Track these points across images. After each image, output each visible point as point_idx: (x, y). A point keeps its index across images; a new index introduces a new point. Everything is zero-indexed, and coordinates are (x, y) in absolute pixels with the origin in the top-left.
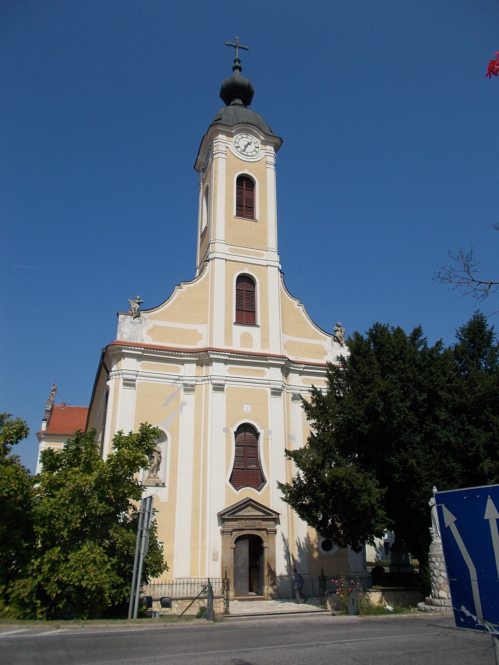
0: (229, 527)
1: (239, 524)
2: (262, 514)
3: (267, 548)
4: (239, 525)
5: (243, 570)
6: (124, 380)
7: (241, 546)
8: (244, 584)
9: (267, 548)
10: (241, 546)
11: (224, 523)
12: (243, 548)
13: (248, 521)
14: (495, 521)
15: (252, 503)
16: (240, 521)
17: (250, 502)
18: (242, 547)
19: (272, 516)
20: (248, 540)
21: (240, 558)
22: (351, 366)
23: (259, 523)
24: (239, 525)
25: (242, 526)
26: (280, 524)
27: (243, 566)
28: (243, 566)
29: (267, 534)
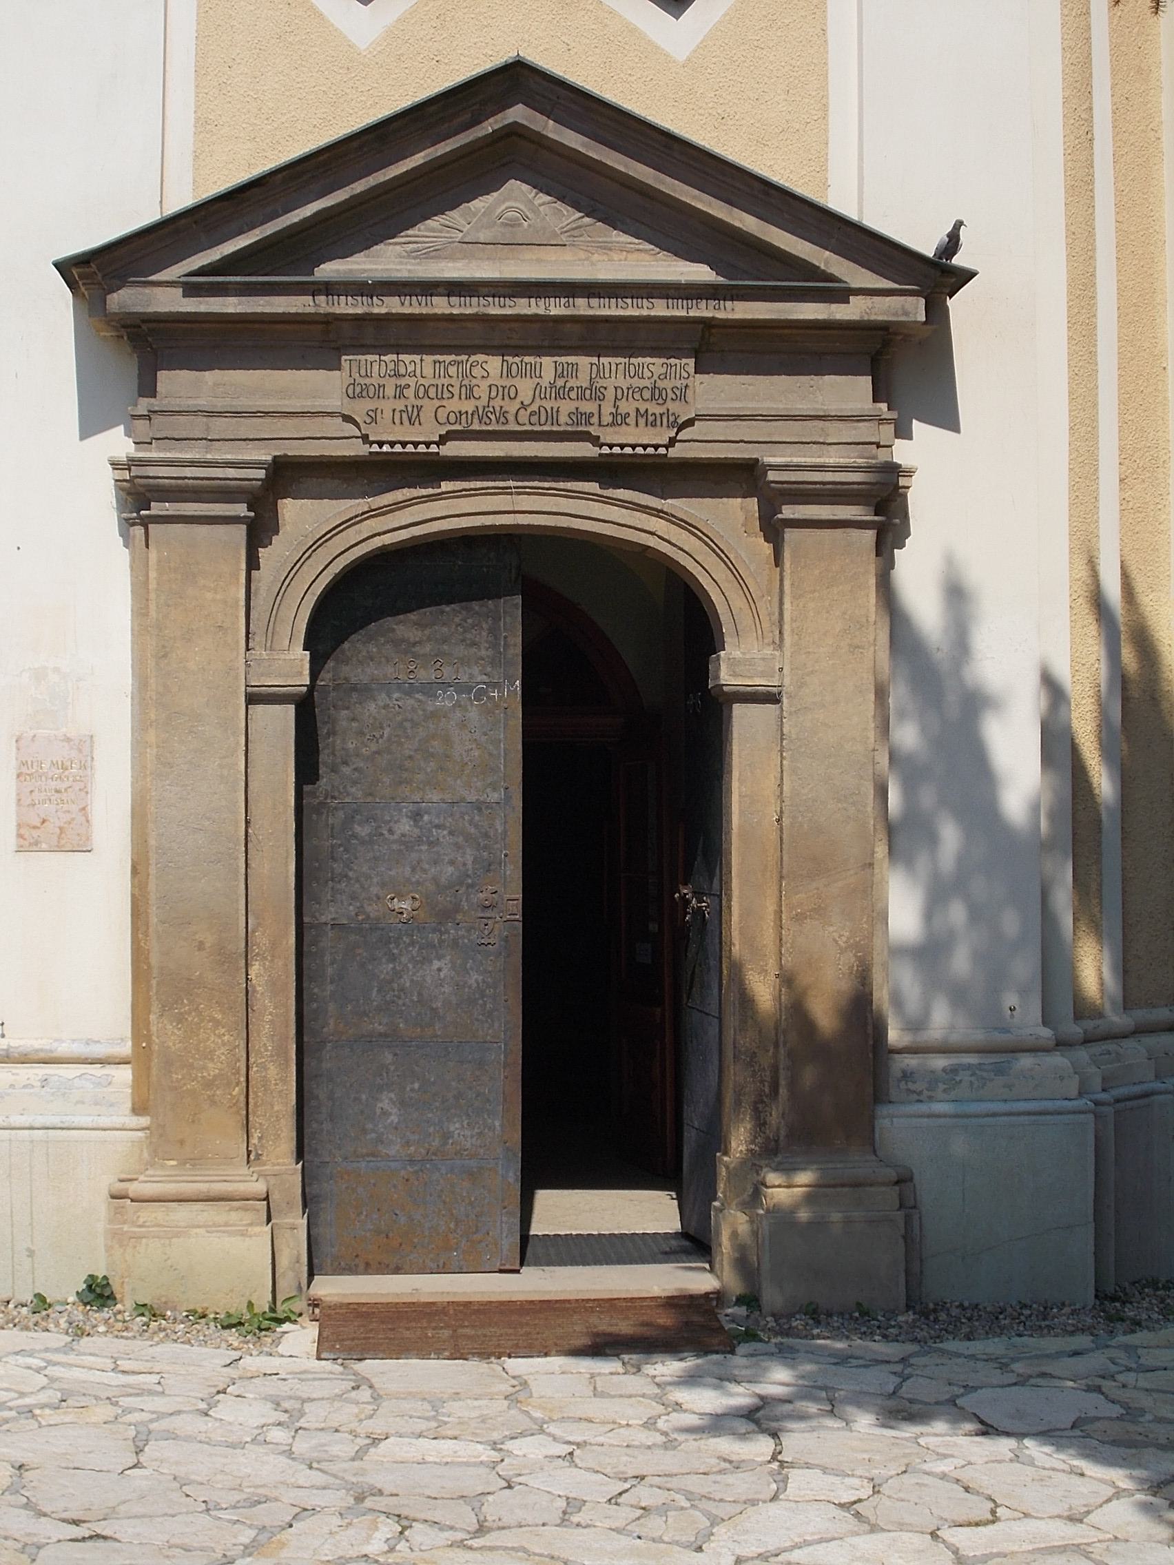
0: (220, 427)
1: (356, 392)
2: (701, 273)
3: (772, 698)
4: (359, 409)
5: (442, 966)
6: (661, 415)
7: (426, 675)
8: (454, 1127)
9: (772, 698)
10: (426, 675)
11: (148, 388)
12: (443, 701)
13: (494, 364)
14: (86, 441)
15: (552, 130)
16: (376, 365)
17: (518, 114)
18: (429, 689)
19: (842, 294)
20: (511, 610)
21: (405, 826)
22: (372, 909)
23: (657, 394)
24: (359, 409)
25: (413, 417)
26: (82, 438)
27: (446, 915)
28: (446, 915)
29: (773, 530)
